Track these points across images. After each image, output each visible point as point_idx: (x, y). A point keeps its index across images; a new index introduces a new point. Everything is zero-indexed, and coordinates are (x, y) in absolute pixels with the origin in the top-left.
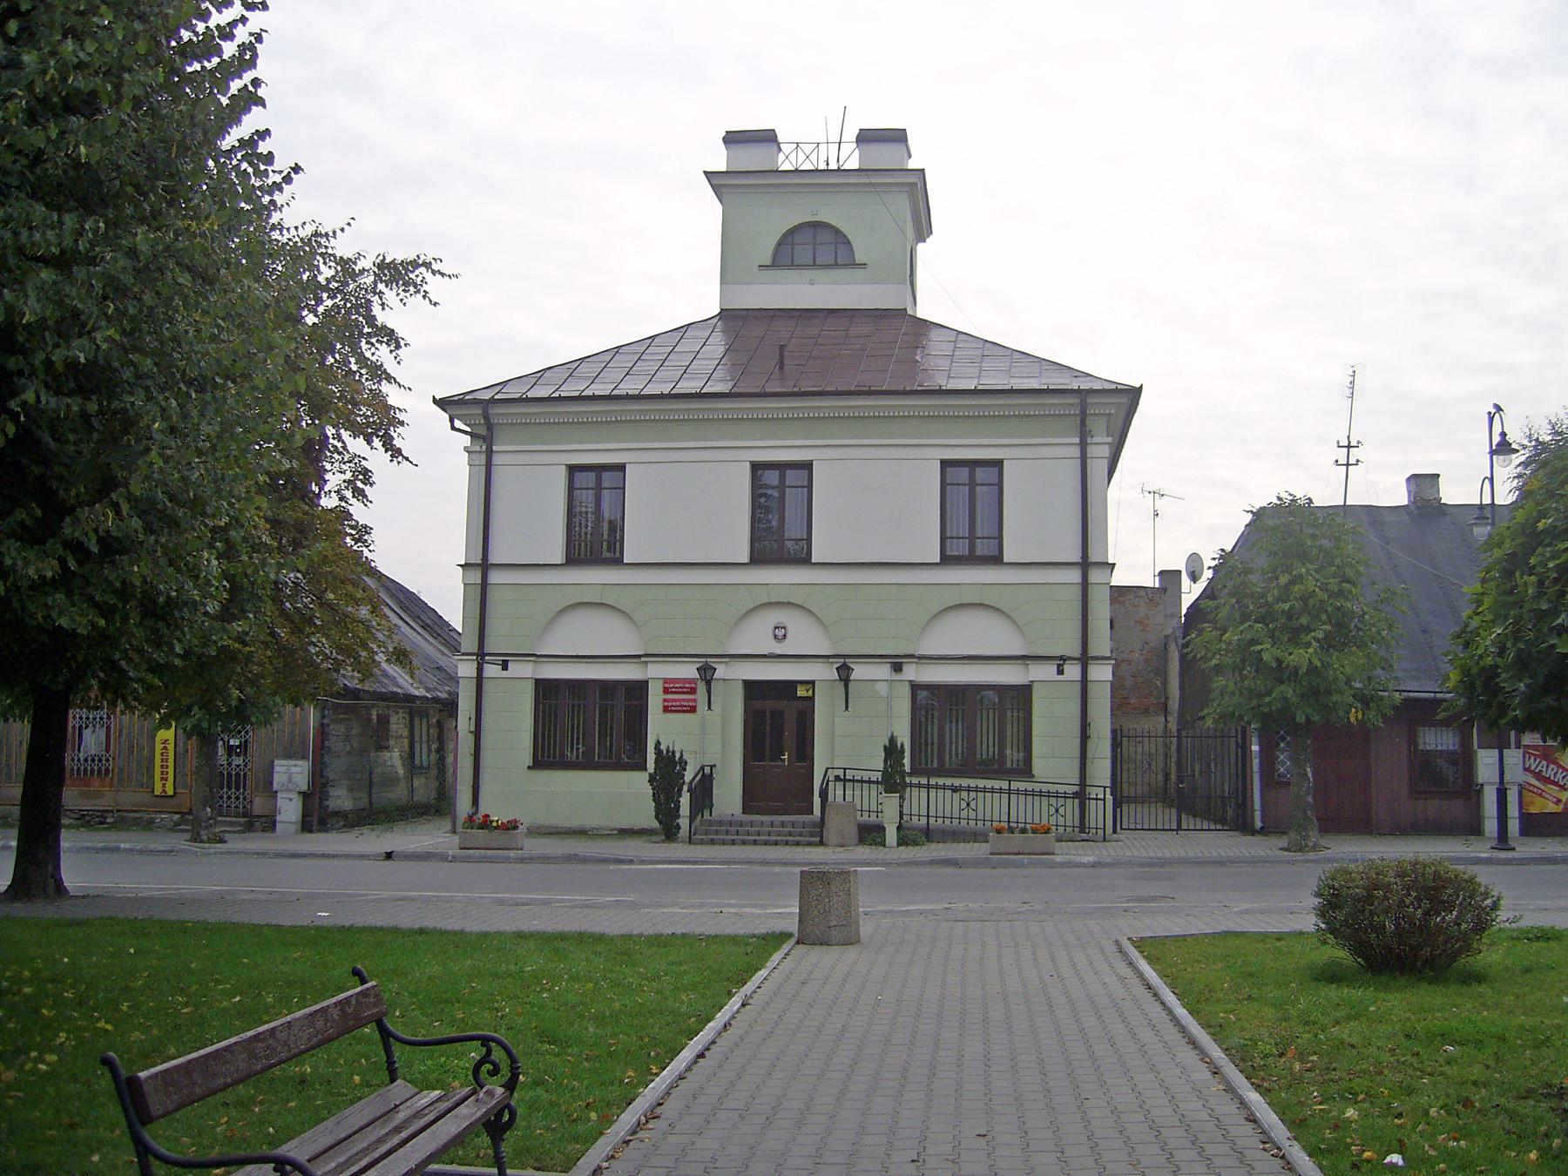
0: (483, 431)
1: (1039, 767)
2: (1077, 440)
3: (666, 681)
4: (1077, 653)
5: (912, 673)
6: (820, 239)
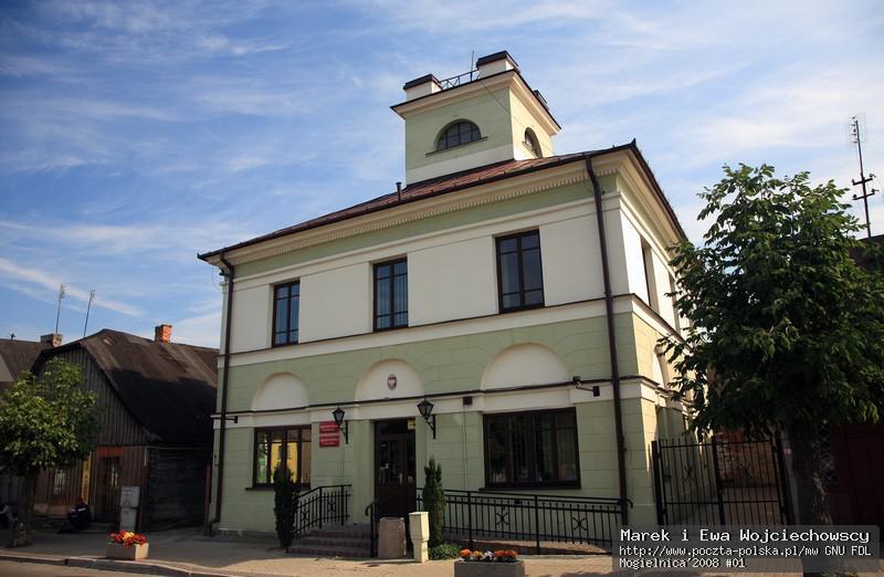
0: (228, 271)
1: (586, 478)
2: (593, 199)
3: (322, 423)
4: (608, 374)
5: (483, 405)
6: (462, 131)
